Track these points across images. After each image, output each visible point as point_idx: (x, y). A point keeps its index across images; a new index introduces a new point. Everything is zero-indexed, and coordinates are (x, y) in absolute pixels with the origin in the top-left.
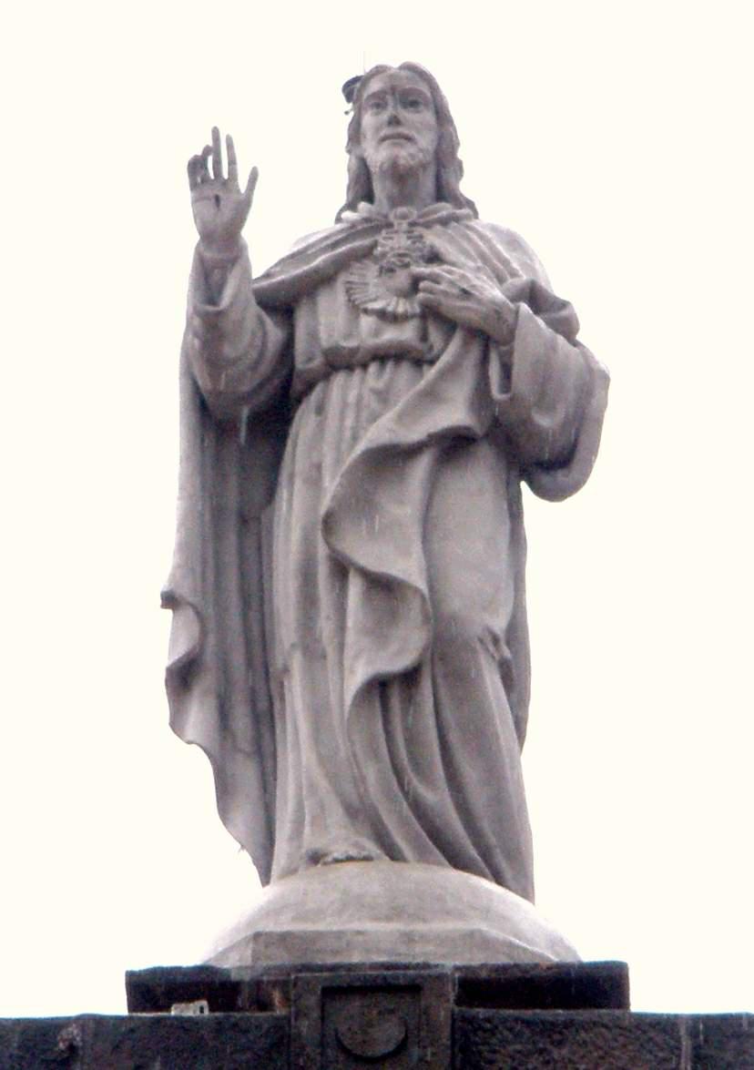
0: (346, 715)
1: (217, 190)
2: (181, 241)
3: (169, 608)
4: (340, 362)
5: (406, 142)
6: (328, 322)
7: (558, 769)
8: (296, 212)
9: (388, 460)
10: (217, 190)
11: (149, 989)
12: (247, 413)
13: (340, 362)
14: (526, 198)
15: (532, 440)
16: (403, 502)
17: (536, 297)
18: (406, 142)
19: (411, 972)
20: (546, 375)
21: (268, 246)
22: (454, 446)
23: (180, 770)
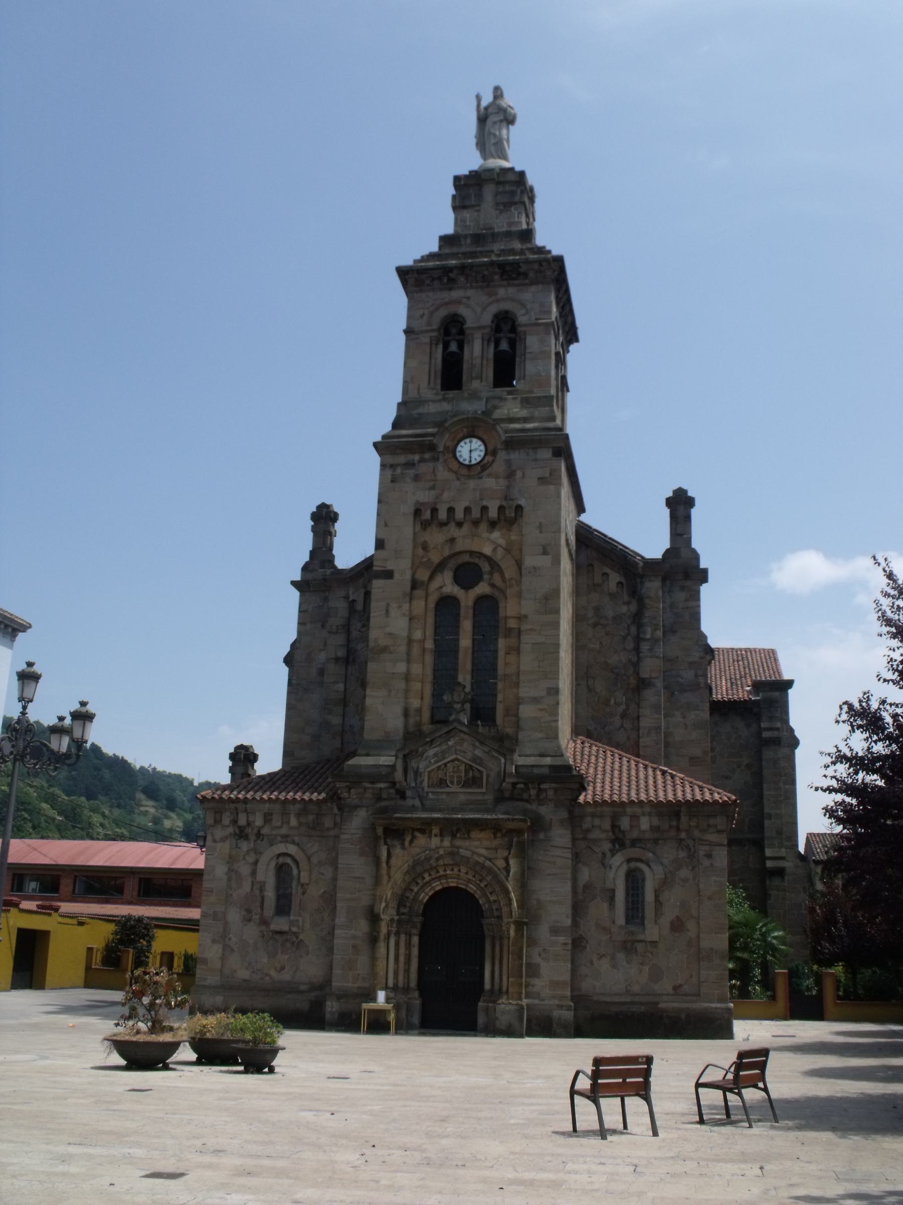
0: (573, 552)
1: (479, 98)
2: (475, 103)
3: (698, 592)
4: (492, 114)
5: (498, 93)
6: (490, 110)
7: (510, 153)
8: (487, 99)
9: (495, 123)
10: (479, 98)
11: (470, 172)
12: (482, 120)
13: (492, 114)
14: (509, 100)
15: (510, 120)
16: (497, 126)
17: (510, 107)
18: (498, 93)
19: (530, 434)
20: (510, 113)
21: (484, 103)
22: (501, 121)
23: (477, 154)
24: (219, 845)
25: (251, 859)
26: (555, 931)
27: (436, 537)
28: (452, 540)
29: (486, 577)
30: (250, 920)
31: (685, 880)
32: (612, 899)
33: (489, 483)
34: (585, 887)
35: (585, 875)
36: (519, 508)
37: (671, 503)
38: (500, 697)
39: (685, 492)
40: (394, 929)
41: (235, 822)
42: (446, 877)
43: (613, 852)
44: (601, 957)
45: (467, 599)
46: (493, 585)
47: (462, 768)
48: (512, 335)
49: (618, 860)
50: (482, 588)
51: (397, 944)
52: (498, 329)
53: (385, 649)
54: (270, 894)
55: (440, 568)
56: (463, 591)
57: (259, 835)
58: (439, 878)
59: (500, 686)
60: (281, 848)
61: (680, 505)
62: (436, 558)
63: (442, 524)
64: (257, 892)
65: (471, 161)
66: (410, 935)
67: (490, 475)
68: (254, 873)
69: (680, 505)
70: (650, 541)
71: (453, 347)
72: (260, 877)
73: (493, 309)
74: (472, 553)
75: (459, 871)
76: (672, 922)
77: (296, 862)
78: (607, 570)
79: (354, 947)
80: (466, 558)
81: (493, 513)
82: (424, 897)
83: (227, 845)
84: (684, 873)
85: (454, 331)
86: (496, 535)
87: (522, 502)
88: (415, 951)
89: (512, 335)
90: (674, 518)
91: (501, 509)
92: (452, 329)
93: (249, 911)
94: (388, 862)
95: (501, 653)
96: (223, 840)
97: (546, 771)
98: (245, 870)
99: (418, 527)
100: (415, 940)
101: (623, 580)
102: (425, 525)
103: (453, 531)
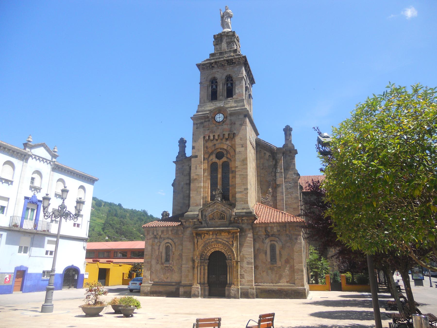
24: (149, 241)
25: (158, 244)
26: (248, 263)
27: (210, 144)
28: (215, 145)
29: (225, 155)
30: (158, 263)
31: (289, 247)
32: (266, 253)
33: (225, 127)
34: (258, 250)
35: (257, 246)
36: (234, 134)
37: (284, 130)
38: (230, 192)
39: (289, 126)
40: (199, 265)
41: (153, 234)
43: (266, 238)
44: (263, 272)
45: (220, 162)
46: (227, 158)
47: (219, 214)
48: (232, 82)
49: (267, 241)
50: (224, 159)
51: (201, 269)
52: (227, 81)
53: (196, 179)
54: (164, 255)
55: (212, 153)
56: (218, 160)
57: (160, 237)
58: (213, 248)
59: (230, 188)
60: (167, 241)
61: (288, 131)
62: (210, 151)
63: (212, 140)
64: (160, 254)
65: (219, 30)
66: (204, 266)
67: (225, 124)
68: (159, 249)
69: (288, 131)
70: (278, 142)
71: (214, 87)
72: (161, 250)
73: (226, 74)
74: (221, 149)
76: (285, 260)
77: (171, 245)
78: (265, 152)
79: (188, 270)
80: (219, 150)
81: (226, 136)
82: (209, 254)
83: (151, 241)
84: (288, 244)
85: (214, 82)
86: (228, 142)
87: (235, 132)
88: (206, 271)
89: (232, 82)
90: (286, 134)
91: (229, 134)
92: (214, 82)
93: (158, 260)
94: (197, 244)
95: (230, 179)
96: (150, 239)
97: (244, 214)
98: (156, 248)
99: (205, 142)
100: (206, 268)
101: (270, 155)
102: (207, 141)
103: (215, 142)
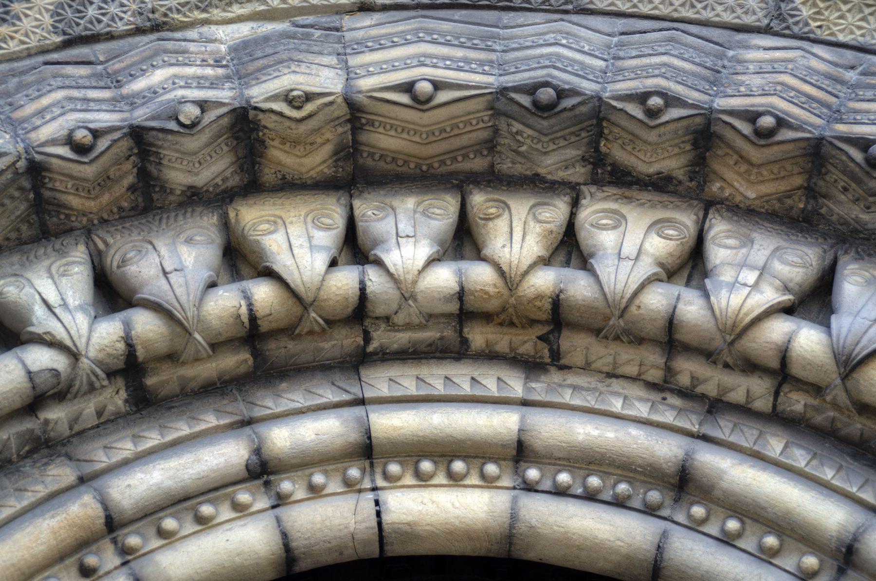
42: (352, 340)
75: (569, 248)
